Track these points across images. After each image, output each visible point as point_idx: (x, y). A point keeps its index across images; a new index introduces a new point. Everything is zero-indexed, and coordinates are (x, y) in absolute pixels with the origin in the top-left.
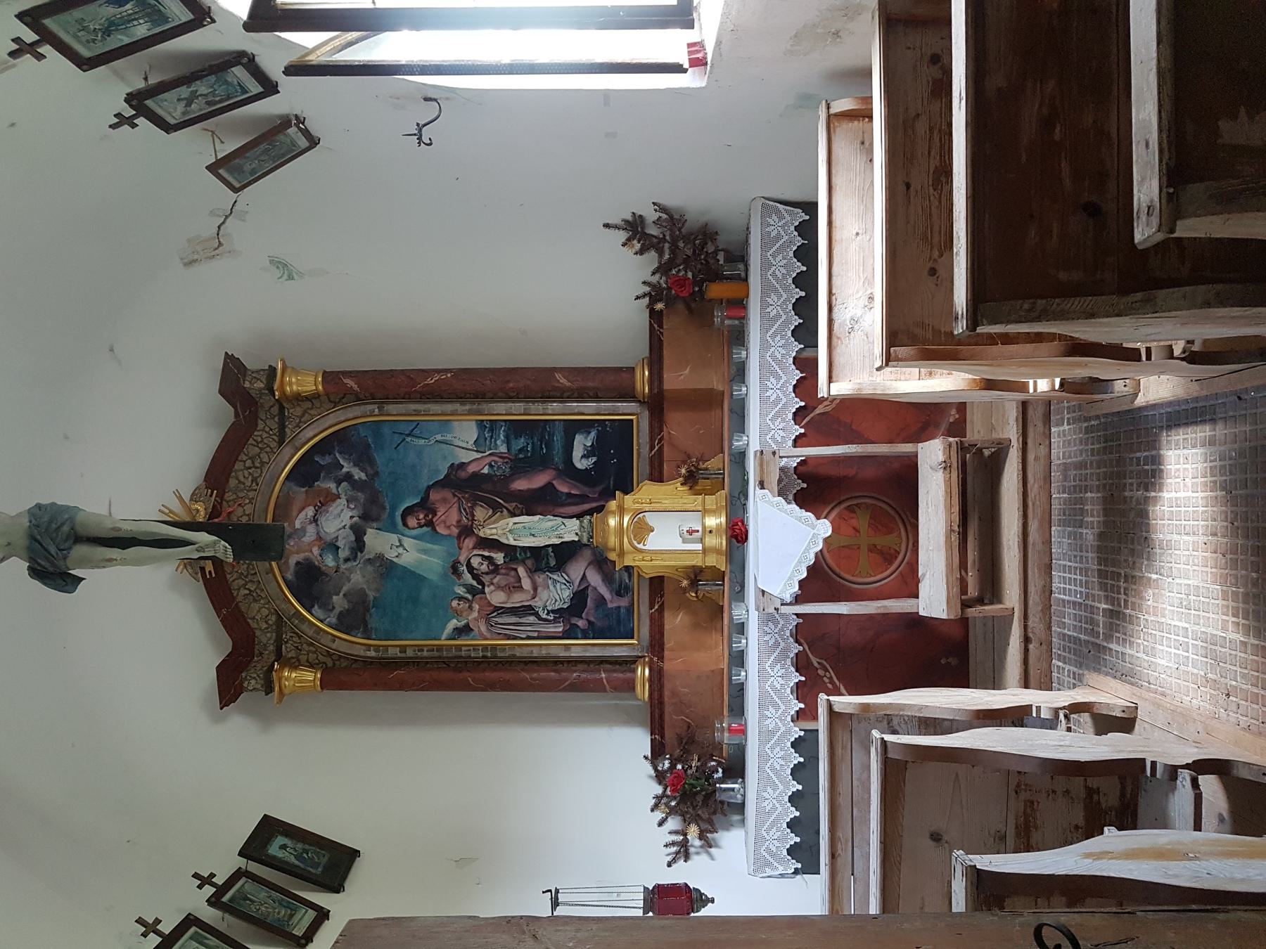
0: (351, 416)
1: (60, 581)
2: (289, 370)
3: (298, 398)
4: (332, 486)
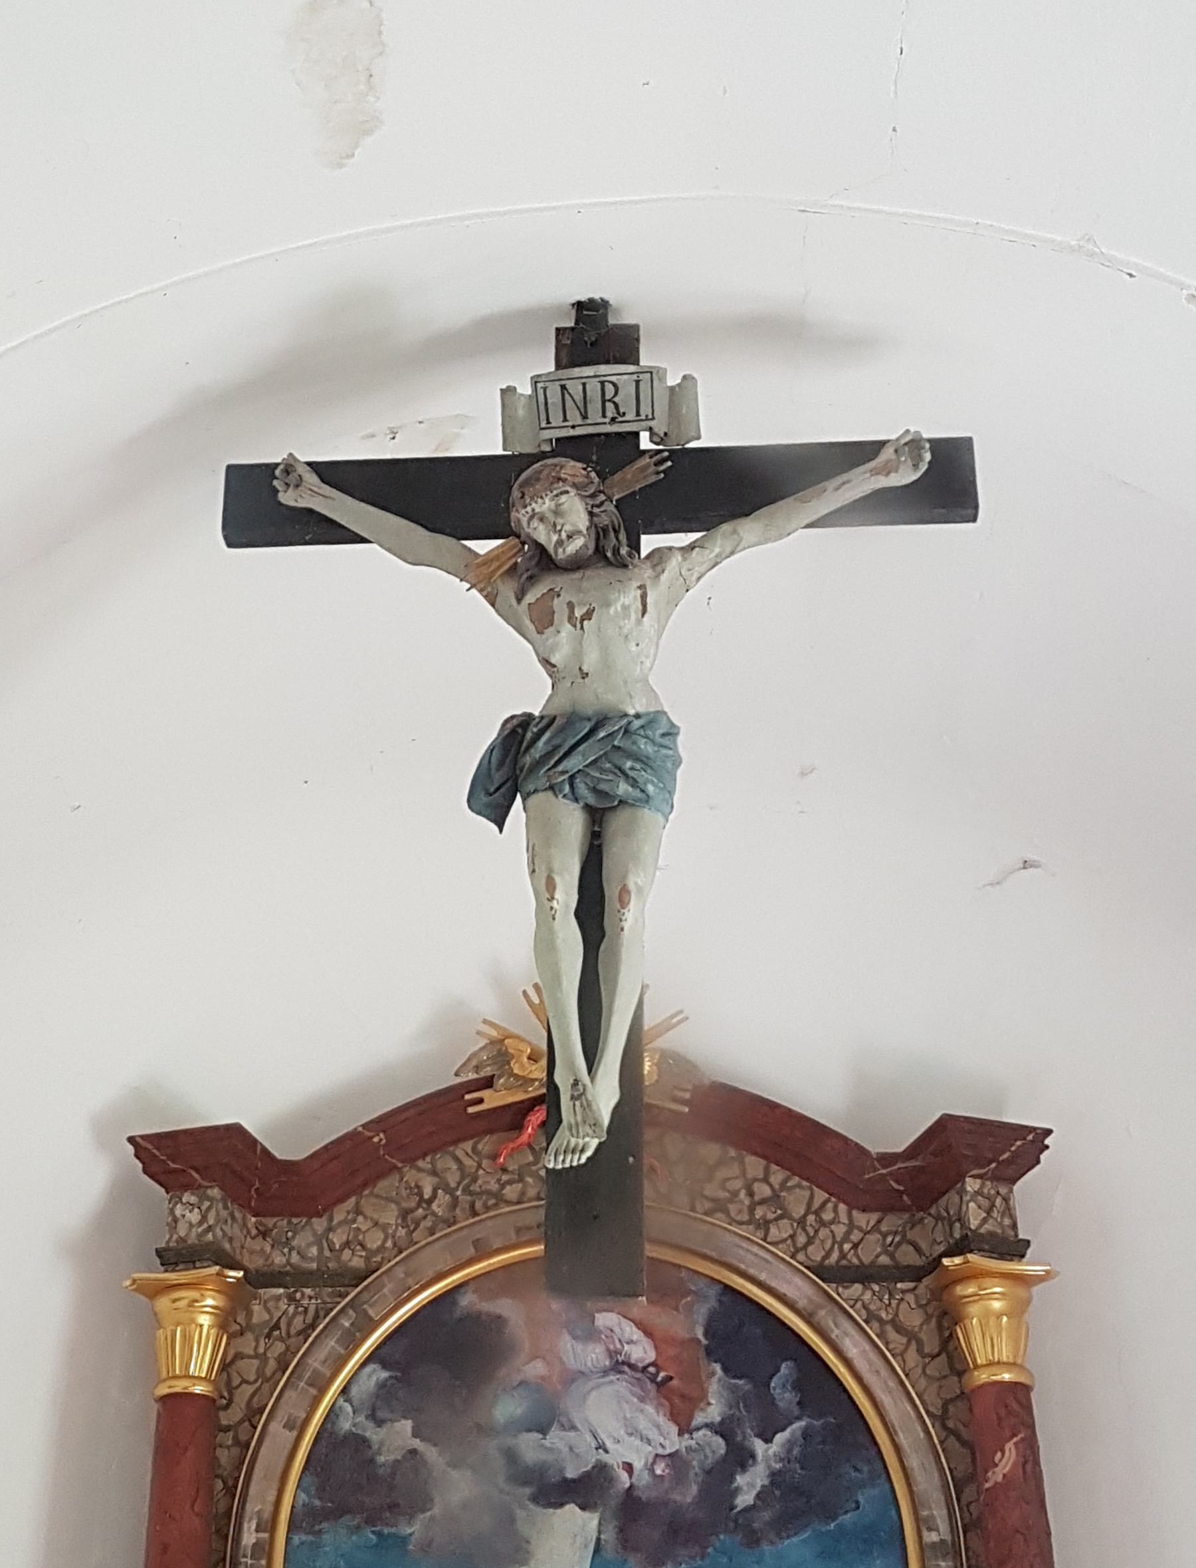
0: (913, 1462)
1: (498, 778)
2: (1021, 1292)
3: (947, 1318)
4: (714, 1411)
